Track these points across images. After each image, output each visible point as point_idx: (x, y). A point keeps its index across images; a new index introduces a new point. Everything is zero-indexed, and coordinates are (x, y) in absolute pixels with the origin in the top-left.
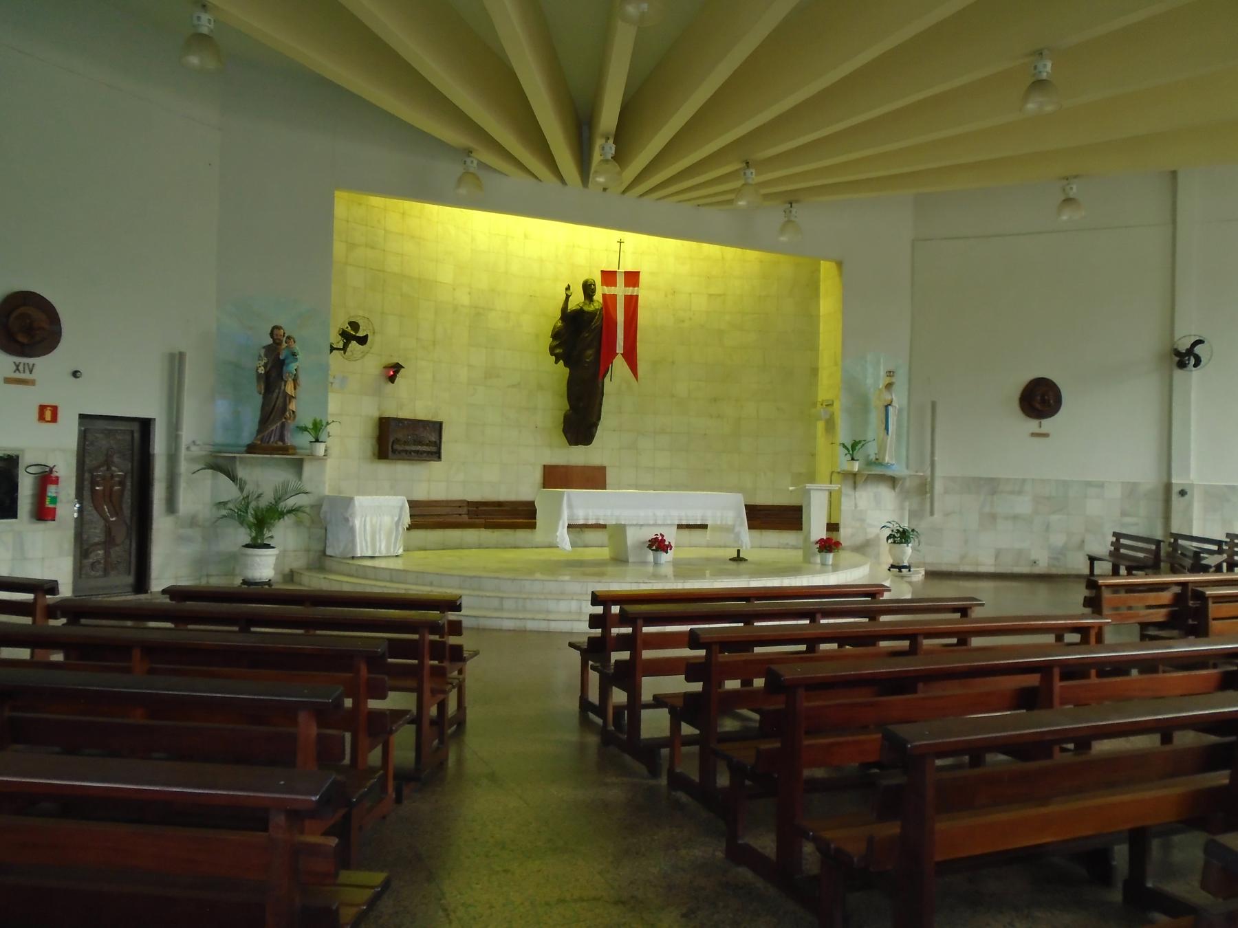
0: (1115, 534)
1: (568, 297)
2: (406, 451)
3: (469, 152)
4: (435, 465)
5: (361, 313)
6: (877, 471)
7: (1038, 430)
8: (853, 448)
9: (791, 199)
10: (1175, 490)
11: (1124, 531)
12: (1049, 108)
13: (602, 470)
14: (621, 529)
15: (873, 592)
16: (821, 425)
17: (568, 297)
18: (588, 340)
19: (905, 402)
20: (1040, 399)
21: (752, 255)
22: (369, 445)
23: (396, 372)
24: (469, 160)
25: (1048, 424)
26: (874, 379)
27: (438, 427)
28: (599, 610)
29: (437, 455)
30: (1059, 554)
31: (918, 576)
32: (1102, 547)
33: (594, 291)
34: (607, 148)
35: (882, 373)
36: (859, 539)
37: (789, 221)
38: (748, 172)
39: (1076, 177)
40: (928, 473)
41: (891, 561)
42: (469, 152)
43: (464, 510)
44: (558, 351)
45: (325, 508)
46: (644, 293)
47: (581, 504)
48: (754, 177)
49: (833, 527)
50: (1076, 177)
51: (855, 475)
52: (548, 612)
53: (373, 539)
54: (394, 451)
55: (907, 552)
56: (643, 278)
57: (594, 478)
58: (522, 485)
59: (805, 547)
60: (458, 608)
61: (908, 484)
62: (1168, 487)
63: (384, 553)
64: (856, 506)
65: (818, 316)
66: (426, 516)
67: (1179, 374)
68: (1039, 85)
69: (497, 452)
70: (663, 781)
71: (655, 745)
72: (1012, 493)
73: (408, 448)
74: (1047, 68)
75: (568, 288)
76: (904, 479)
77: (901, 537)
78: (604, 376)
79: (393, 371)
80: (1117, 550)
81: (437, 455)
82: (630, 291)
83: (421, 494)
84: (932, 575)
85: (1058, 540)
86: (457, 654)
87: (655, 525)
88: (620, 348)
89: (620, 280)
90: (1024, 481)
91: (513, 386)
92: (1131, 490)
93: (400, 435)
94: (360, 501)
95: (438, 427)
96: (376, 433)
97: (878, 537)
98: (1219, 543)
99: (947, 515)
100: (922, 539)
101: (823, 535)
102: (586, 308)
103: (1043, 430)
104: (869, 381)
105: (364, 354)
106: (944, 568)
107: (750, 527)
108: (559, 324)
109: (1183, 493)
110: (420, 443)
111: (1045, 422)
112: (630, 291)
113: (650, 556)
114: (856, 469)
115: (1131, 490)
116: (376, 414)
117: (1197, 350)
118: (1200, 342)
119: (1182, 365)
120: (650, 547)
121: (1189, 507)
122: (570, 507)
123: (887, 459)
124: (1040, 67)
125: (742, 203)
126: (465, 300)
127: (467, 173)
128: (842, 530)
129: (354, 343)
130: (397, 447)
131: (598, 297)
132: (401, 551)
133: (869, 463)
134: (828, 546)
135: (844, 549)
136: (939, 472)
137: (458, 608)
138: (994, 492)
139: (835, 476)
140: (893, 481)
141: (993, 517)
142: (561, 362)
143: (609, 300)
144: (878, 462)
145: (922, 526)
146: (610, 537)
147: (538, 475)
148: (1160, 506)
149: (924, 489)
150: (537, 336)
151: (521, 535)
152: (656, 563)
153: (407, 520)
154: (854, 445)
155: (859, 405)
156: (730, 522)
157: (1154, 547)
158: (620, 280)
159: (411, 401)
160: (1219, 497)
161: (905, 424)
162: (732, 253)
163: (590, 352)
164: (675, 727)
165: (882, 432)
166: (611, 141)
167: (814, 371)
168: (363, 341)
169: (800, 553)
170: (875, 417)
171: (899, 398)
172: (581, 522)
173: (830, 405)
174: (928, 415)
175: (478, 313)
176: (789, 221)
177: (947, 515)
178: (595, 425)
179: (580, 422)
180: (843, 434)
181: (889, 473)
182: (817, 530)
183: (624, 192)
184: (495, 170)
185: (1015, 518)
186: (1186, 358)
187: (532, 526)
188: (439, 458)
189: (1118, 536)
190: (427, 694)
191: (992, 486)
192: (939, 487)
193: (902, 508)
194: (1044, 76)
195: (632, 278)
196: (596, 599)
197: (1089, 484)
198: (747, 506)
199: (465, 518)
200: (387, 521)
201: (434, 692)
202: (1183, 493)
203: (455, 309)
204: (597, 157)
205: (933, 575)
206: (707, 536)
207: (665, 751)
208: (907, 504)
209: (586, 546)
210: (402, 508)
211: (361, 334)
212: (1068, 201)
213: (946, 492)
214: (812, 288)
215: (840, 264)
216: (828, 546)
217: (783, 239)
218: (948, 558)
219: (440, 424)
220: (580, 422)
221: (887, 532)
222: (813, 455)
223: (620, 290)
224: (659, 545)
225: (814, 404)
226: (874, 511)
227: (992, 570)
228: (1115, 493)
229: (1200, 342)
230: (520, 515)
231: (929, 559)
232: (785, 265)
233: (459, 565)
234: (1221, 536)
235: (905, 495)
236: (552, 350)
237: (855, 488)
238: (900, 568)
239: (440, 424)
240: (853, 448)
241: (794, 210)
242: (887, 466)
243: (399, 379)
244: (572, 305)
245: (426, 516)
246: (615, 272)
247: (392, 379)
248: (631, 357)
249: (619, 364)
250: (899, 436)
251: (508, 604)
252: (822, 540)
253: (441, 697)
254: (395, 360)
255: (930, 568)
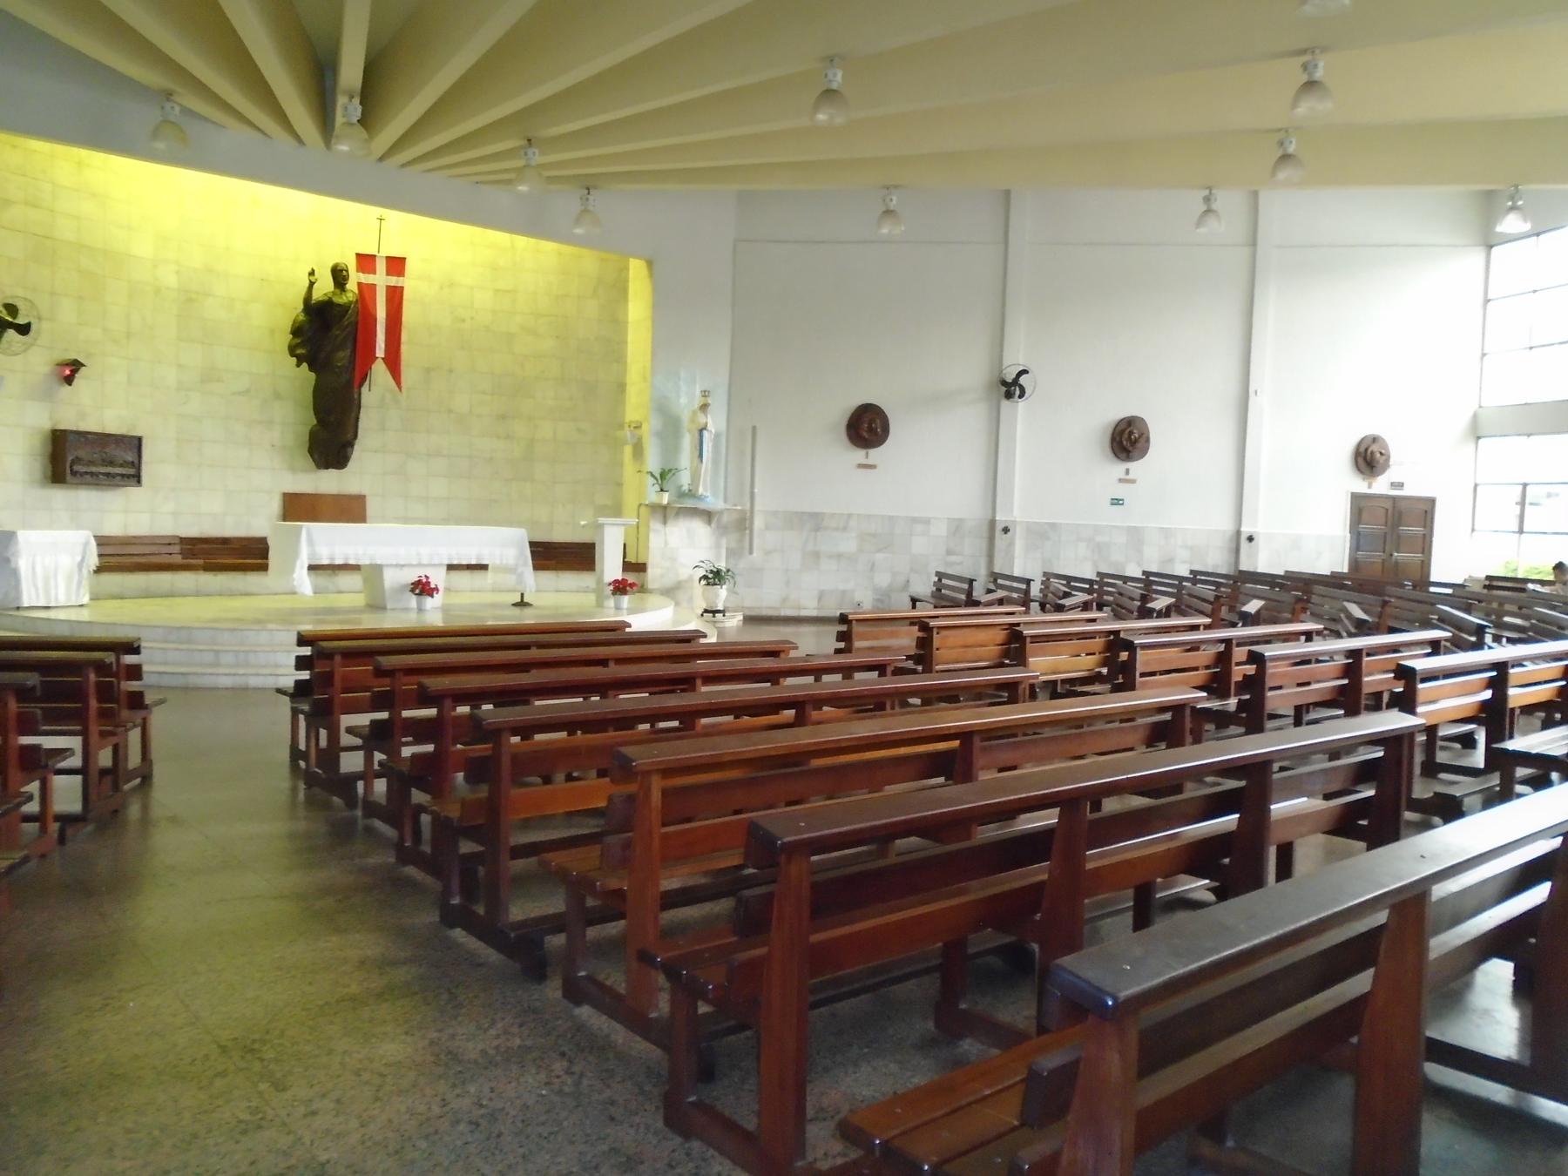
0: (938, 574)
1: (312, 284)
2: (92, 474)
3: (168, 95)
4: (132, 492)
5: (20, 292)
6: (689, 503)
7: (864, 461)
8: (664, 477)
9: (588, 186)
10: (999, 527)
11: (950, 572)
12: (839, 120)
13: (361, 499)
14: (376, 570)
15: (688, 638)
16: (628, 450)
17: (312, 284)
18: (337, 341)
19: (723, 426)
20: (867, 427)
21: (549, 246)
22: (38, 465)
23: (74, 372)
24: (168, 105)
25: (875, 454)
26: (685, 402)
27: (136, 443)
28: (306, 651)
29: (136, 479)
30: (883, 595)
31: (733, 622)
32: (924, 588)
33: (346, 278)
34: (350, 108)
35: (698, 393)
36: (669, 581)
37: (586, 211)
38: (530, 151)
39: (896, 187)
40: (748, 506)
41: (704, 606)
42: (168, 95)
43: (177, 549)
44: (299, 351)
45: (1082, 1065)
46: (410, 284)
47: (327, 540)
48: (537, 158)
49: (635, 567)
50: (896, 187)
51: (665, 508)
52: (277, 666)
53: (47, 584)
54: (74, 473)
55: (721, 595)
56: (410, 267)
57: (350, 509)
58: (255, 516)
59: (598, 592)
60: (136, 650)
61: (725, 518)
62: (992, 523)
63: (62, 601)
64: (666, 543)
65: (626, 322)
66: (119, 557)
67: (1005, 403)
68: (829, 95)
69: (216, 473)
70: (359, 813)
71: (353, 778)
72: (837, 529)
73: (94, 469)
74: (837, 78)
75: (312, 273)
76: (721, 513)
77: (715, 577)
78: (361, 385)
79: (70, 371)
80: (939, 590)
81: (136, 479)
82: (393, 281)
83: (116, 526)
84: (752, 620)
85: (883, 580)
86: (136, 701)
87: (420, 565)
88: (380, 352)
89: (381, 266)
90: (850, 516)
91: (239, 393)
92: (957, 527)
93: (82, 453)
94: (24, 536)
95: (136, 443)
96: (49, 449)
97: (691, 578)
98: (1090, 582)
99: (768, 553)
100: (738, 579)
101: (619, 576)
102: (337, 300)
103: (870, 462)
104: (683, 400)
105: (27, 347)
106: (765, 613)
107: (537, 567)
108: (302, 317)
109: (1250, 539)
110: (111, 463)
111: (873, 452)
112: (393, 281)
113: (413, 601)
114: (665, 502)
115: (957, 527)
116: (47, 425)
117: (1023, 380)
118: (1025, 372)
119: (1009, 395)
120: (412, 591)
121: (1011, 544)
122: (311, 542)
123: (701, 491)
124: (830, 76)
125: (523, 188)
126: (170, 279)
127: (166, 121)
128: (650, 570)
129: (11, 333)
130: (77, 468)
131: (352, 285)
132: (86, 600)
133: (682, 495)
134: (620, 588)
135: (650, 592)
136: (757, 507)
137: (136, 650)
138: (817, 529)
139: (643, 509)
140: (708, 516)
141: (817, 555)
142: (305, 365)
143: (367, 291)
144: (691, 494)
145: (741, 565)
146: (365, 581)
147: (276, 505)
148: (984, 544)
149: (743, 524)
150: (272, 332)
151: (251, 580)
152: (420, 610)
153: (93, 561)
154: (663, 475)
155: (670, 429)
156: (511, 561)
157: (966, 586)
158: (381, 266)
159: (94, 409)
160: (1041, 534)
161: (723, 450)
162: (523, 243)
163: (341, 354)
164: (369, 759)
165: (696, 460)
166: (357, 101)
167: (621, 387)
168: (24, 329)
169: (592, 597)
170: (687, 442)
171: (715, 422)
172: (325, 562)
173: (638, 427)
174: (746, 440)
175: (189, 299)
176: (586, 211)
177: (768, 553)
178: (350, 444)
179: (331, 439)
180: (653, 462)
181: (701, 506)
182: (611, 567)
183: (381, 159)
184: (206, 120)
185: (839, 556)
186: (1011, 388)
187: (264, 568)
188: (139, 482)
189: (940, 575)
190: (94, 738)
191: (815, 522)
192: (758, 523)
193: (718, 546)
194: (834, 86)
195: (396, 265)
196: (302, 640)
197: (915, 520)
198: (532, 544)
199: (178, 559)
200: (67, 562)
201: (103, 734)
202: (1006, 530)
203: (158, 291)
204: (339, 119)
205: (752, 620)
206: (488, 578)
207: (360, 785)
208: (724, 541)
209: (340, 592)
210: (86, 544)
211: (21, 320)
212: (888, 212)
213: (767, 528)
214: (620, 290)
215: (650, 264)
216: (620, 588)
217: (579, 231)
218: (769, 599)
219: (140, 439)
220: (331, 439)
221: (702, 573)
222: (620, 485)
223: (381, 279)
224: (423, 588)
225: (621, 426)
226: (682, 549)
227: (814, 613)
228: (940, 529)
229: (1025, 372)
230: (248, 555)
231: (747, 603)
232: (588, 261)
233: (170, 618)
234: (1091, 575)
235: (722, 530)
236: (292, 350)
237: (665, 523)
238: (714, 612)
239: (140, 439)
240: (664, 477)
241: (591, 198)
242: (700, 498)
243: (79, 379)
244: (318, 295)
245: (119, 557)
246: (374, 256)
247: (69, 380)
248: (393, 363)
249: (379, 370)
250: (715, 462)
251: (227, 659)
252: (616, 581)
253: (114, 740)
254: (73, 356)
255: (749, 613)
